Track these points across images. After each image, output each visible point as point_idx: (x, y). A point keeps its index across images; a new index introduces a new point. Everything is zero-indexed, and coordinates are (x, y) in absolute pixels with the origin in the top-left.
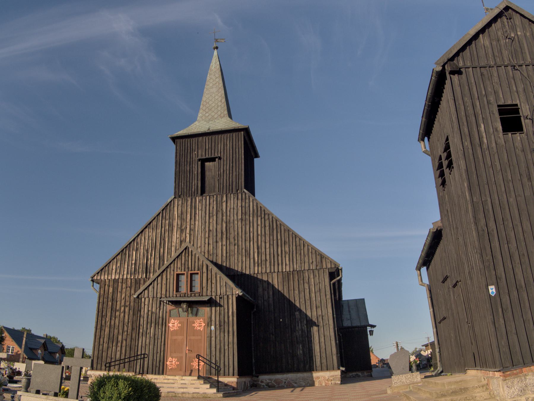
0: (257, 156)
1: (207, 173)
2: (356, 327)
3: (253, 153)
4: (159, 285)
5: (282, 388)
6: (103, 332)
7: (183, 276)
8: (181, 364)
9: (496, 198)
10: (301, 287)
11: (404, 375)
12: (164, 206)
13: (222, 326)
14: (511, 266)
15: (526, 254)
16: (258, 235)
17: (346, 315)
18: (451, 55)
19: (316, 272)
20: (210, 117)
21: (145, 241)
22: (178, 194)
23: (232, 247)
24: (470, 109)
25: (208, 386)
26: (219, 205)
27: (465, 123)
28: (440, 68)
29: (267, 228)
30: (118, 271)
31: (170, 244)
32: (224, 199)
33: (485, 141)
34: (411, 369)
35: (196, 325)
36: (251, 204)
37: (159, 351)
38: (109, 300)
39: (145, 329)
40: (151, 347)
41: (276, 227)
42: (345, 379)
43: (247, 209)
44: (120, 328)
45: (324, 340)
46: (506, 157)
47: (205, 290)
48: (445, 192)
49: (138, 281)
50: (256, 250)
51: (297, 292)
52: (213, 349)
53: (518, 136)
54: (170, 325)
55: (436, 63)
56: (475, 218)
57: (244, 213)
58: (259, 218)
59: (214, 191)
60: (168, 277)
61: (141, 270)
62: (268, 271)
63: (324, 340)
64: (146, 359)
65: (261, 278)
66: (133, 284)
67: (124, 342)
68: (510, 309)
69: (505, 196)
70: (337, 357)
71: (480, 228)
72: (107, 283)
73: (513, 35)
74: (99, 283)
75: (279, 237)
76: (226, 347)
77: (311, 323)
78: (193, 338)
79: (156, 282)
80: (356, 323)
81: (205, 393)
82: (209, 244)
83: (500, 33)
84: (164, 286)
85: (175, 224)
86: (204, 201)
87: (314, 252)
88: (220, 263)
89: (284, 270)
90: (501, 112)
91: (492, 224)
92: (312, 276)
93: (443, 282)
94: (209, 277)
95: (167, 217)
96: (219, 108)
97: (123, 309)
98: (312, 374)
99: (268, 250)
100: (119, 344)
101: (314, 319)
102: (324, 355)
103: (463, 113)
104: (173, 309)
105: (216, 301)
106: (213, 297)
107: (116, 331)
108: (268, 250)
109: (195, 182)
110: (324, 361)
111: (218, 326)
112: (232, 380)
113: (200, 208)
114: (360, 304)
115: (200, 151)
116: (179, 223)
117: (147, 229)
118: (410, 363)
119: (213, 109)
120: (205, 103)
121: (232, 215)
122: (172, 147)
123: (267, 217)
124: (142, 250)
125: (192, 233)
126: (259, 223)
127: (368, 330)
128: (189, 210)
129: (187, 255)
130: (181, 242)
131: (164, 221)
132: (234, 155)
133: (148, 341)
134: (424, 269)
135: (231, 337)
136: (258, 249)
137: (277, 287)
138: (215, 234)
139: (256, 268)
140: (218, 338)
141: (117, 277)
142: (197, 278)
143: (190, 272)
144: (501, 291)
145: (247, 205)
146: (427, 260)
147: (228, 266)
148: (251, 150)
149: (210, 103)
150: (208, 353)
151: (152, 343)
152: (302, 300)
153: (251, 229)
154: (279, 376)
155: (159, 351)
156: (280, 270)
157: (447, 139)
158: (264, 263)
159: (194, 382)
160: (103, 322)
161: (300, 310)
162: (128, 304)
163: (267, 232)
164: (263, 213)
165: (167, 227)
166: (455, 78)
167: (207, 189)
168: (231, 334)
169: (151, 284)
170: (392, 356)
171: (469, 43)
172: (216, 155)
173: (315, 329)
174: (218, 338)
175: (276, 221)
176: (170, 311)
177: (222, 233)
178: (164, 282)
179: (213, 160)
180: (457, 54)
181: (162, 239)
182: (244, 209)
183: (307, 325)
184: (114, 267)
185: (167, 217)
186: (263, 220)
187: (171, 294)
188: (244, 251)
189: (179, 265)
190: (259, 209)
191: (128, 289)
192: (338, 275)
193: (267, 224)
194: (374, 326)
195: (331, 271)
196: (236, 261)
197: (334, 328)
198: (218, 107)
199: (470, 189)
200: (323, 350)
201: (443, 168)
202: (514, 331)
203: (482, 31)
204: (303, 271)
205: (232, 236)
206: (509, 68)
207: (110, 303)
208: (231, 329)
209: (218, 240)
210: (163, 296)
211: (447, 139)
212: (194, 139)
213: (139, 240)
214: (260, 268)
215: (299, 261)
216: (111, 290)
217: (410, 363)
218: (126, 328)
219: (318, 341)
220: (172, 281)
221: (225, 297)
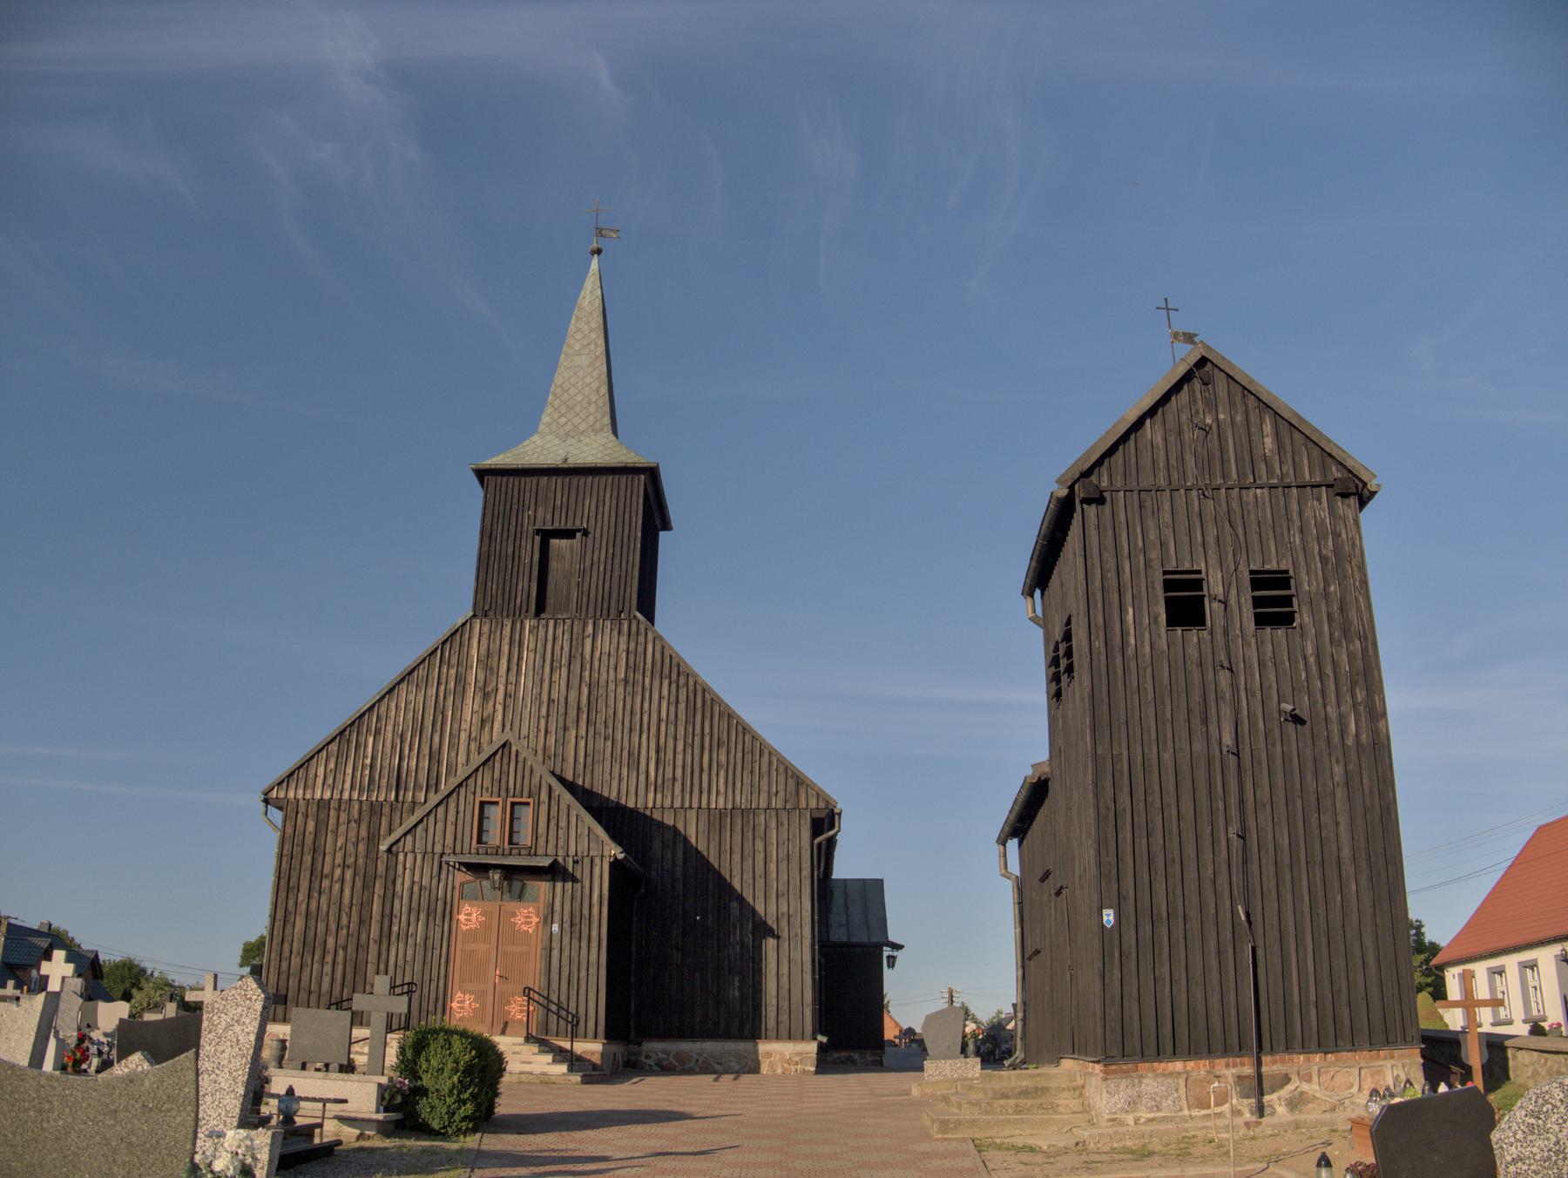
0: (666, 526)
2: (859, 945)
3: (658, 522)
4: (440, 825)
5: (691, 1072)
6: (289, 927)
7: (493, 808)
8: (483, 1006)
9: (1139, 751)
10: (748, 846)
11: (949, 1062)
12: (445, 631)
13: (575, 924)
14: (1147, 879)
15: (1177, 860)
16: (660, 720)
17: (837, 915)
18: (1088, 465)
19: (784, 815)
20: (568, 427)
21: (397, 714)
22: (482, 609)
23: (600, 743)
24: (1111, 575)
25: (549, 1058)
26: (576, 641)
27: (1100, 605)
28: (1064, 492)
29: (682, 706)
30: (330, 781)
31: (456, 726)
32: (590, 629)
33: (1132, 641)
34: (963, 1051)
35: (519, 920)
36: (650, 646)
37: (435, 976)
38: (306, 849)
39: (404, 924)
40: (418, 966)
41: (702, 705)
42: (827, 1062)
43: (640, 659)
44: (332, 918)
45: (788, 971)
46: (1166, 674)
47: (542, 841)
48: (1060, 712)
49: (377, 808)
50: (653, 755)
51: (737, 857)
52: (555, 976)
53: (1193, 635)
54: (462, 917)
55: (1058, 481)
56: (1096, 785)
58: (666, 682)
59: (567, 609)
60: (462, 808)
61: (384, 781)
63: (788, 971)
64: (416, 996)
66: (366, 815)
67: (341, 953)
68: (1134, 954)
69: (1155, 750)
70: (813, 1010)
71: (1101, 805)
72: (302, 809)
73: (1209, 421)
74: (280, 808)
75: (707, 730)
76: (583, 974)
77: (763, 930)
78: (510, 948)
79: (432, 818)
80: (859, 937)
81: (545, 1074)
82: (546, 732)
83: (1184, 417)
84: (450, 829)
87: (782, 769)
88: (570, 778)
89: (713, 806)
90: (1168, 585)
91: (1124, 799)
92: (773, 824)
93: (1043, 880)
94: (554, 812)
95: (454, 661)
96: (592, 408)
97: (338, 872)
98: (756, 1046)
99: (680, 757)
100: (329, 958)
101: (771, 922)
102: (785, 1004)
103: (1098, 584)
104: (468, 882)
105: (565, 870)
106: (560, 860)
107: (321, 926)
108: (680, 757)
109: (523, 583)
110: (784, 1018)
111: (566, 926)
112: (591, 1048)
113: (532, 646)
114: (872, 891)
115: (540, 510)
116: (481, 677)
117: (404, 686)
118: (964, 1036)
119: (578, 409)
120: (559, 391)
121: (604, 670)
122: (474, 495)
123: (682, 680)
124: (390, 735)
125: (510, 702)
126: (665, 692)
127: (885, 954)
128: (506, 648)
129: (506, 760)
130: (483, 721)
131: (445, 670)
132: (620, 529)
133: (410, 952)
134: (1013, 844)
135: (594, 951)
136: (658, 752)
137: (693, 841)
138: (562, 710)
139: (651, 796)
140: (566, 953)
141: (327, 795)
142: (526, 814)
143: (510, 800)
144: (1124, 921)
145: (640, 649)
147: (587, 786)
148: (656, 514)
150: (544, 984)
151: (420, 957)
152: (748, 876)
153: (646, 706)
154: (685, 1046)
155: (435, 976)
156: (704, 805)
157: (1069, 622)
158: (668, 784)
159: (518, 1049)
160: (291, 903)
161: (741, 899)
162: (350, 860)
163: (682, 716)
164: (675, 670)
166: (1091, 510)
168: (594, 944)
169: (421, 821)
170: (931, 1019)
171: (1124, 438)
172: (578, 525)
173: (771, 943)
174: (566, 953)
175: (704, 691)
176: (462, 884)
177: (579, 708)
178: (451, 818)
179: (569, 534)
180: (1099, 462)
181: (439, 711)
182: (632, 657)
183: (753, 933)
184: (321, 771)
185: (454, 661)
186: (674, 686)
187: (466, 846)
188: (625, 753)
189: (487, 783)
190: (667, 661)
191: (353, 825)
192: (832, 827)
193: (683, 698)
195: (816, 815)
196: (607, 776)
197: (813, 945)
199: (1094, 732)
200: (784, 992)
201: (1060, 666)
202: (1135, 994)
203: (1151, 412)
204: (755, 811)
205: (601, 717)
206: (1194, 493)
207: (308, 859)
208: (594, 933)
209: (569, 724)
210: (447, 851)
211: (1069, 622)
212: (529, 479)
213: (383, 708)
214: (659, 796)
215: (747, 788)
216: (311, 825)
217: (964, 1036)
218: (344, 920)
219: (774, 972)
220: (468, 817)
221: (587, 861)
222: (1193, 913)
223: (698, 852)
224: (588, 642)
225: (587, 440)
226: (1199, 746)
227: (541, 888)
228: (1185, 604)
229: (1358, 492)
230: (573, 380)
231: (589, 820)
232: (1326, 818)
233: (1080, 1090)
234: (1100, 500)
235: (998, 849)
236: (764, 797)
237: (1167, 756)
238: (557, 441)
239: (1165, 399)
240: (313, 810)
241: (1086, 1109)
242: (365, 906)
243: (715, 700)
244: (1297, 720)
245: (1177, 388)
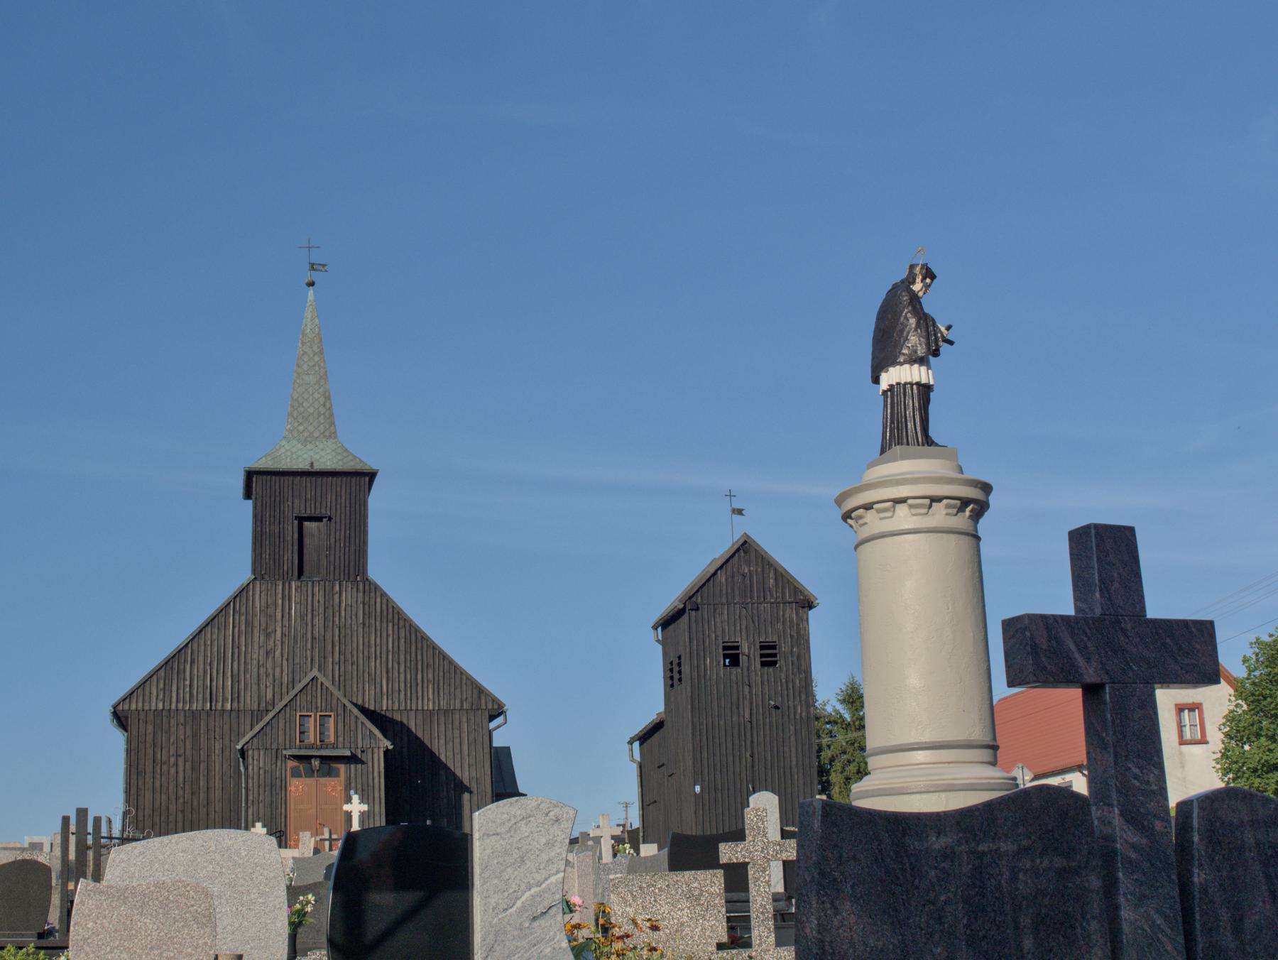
1: (307, 541)
6: (141, 799)
20: (306, 434)
28: (681, 606)
29: (402, 641)
47: (341, 739)
51: (442, 742)
58: (390, 625)
62: (402, 707)
72: (142, 716)
77: (461, 788)
85: (257, 623)
86: (304, 589)
92: (464, 719)
95: (243, 610)
97: (172, 760)
99: (402, 676)
101: (466, 782)
108: (402, 676)
115: (296, 501)
117: (209, 628)
119: (311, 419)
123: (401, 623)
130: (267, 653)
134: (636, 744)
149: (306, 405)
152: (450, 754)
161: (446, 768)
163: (402, 648)
165: (243, 627)
166: (693, 613)
167: (306, 568)
171: (709, 580)
179: (319, 519)
191: (181, 727)
193: (402, 635)
198: (319, 415)
203: (721, 567)
207: (150, 752)
208: (377, 795)
213: (195, 645)
216: (150, 728)
218: (181, 792)
222: (732, 787)
223: (417, 737)
224: (337, 597)
225: (321, 446)
226: (735, 719)
227: (342, 768)
228: (733, 657)
229: (810, 605)
230: (306, 396)
232: (787, 749)
235: (627, 747)
236: (458, 702)
237: (722, 723)
238: (299, 446)
240: (151, 717)
243: (424, 638)
244: (776, 707)
245: (734, 554)
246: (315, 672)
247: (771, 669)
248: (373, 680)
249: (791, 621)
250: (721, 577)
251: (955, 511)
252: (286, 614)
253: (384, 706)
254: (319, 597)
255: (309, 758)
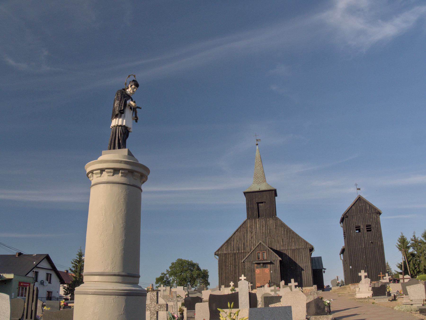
1: (260, 208)
10: (299, 255)
13: (275, 271)
22: (249, 217)
26: (266, 222)
57: (276, 226)
63: (307, 274)
65: (93, 182)
80: (318, 268)
130: (252, 238)
134: (342, 255)
146: (342, 221)
167: (260, 215)
173: (303, 271)
179: (262, 203)
181: (244, 236)
194: (325, 269)
205: (272, 235)
207: (224, 264)
216: (224, 258)
227: (269, 265)
229: (380, 214)
231: (275, 254)
233: (350, 287)
234: (347, 217)
239: (355, 203)
240: (224, 255)
241: (350, 289)
242: (235, 270)
244: (372, 243)
245: (356, 201)
246: (260, 242)
247: (370, 232)
248: (278, 242)
249: (375, 218)
250: (353, 208)
251: (112, 174)
252: (256, 227)
253: (278, 249)
254: (264, 222)
255: (260, 263)
